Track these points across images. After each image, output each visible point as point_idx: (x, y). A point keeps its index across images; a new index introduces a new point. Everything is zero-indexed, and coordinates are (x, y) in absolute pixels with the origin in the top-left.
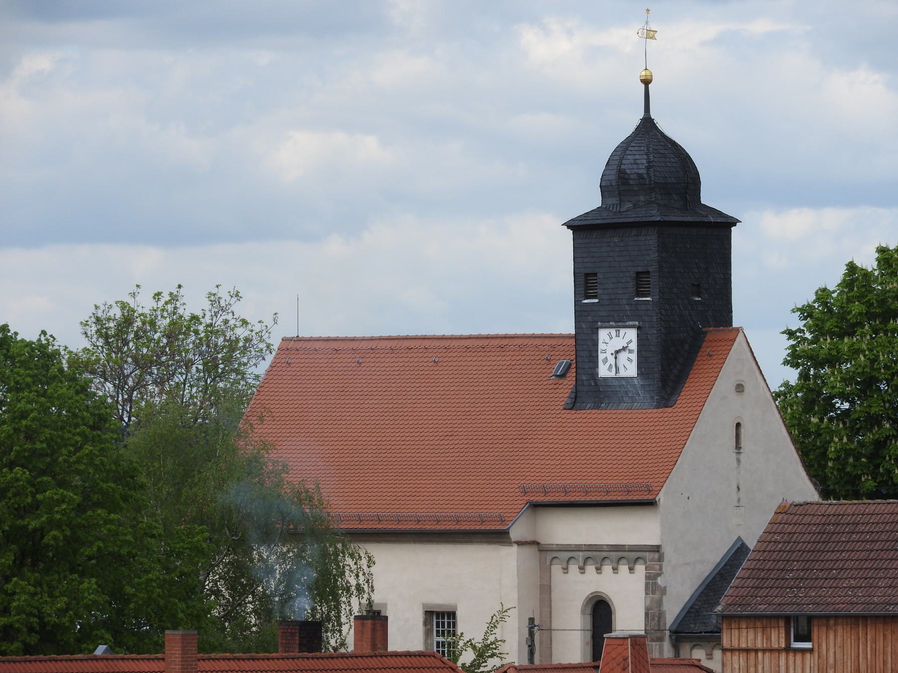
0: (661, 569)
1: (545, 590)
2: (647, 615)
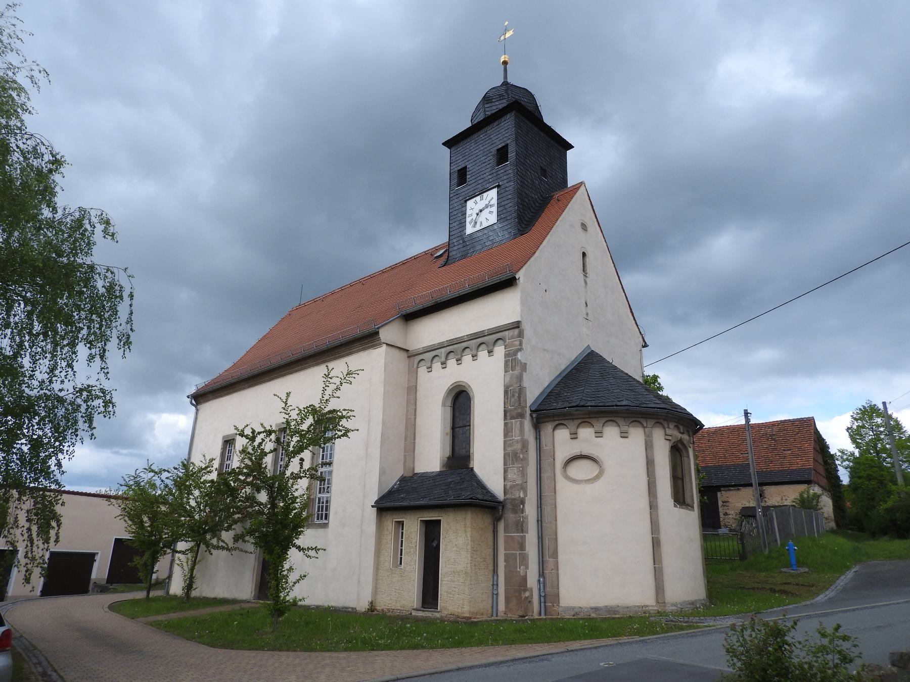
0: (521, 344)
1: (412, 390)
2: (506, 392)
